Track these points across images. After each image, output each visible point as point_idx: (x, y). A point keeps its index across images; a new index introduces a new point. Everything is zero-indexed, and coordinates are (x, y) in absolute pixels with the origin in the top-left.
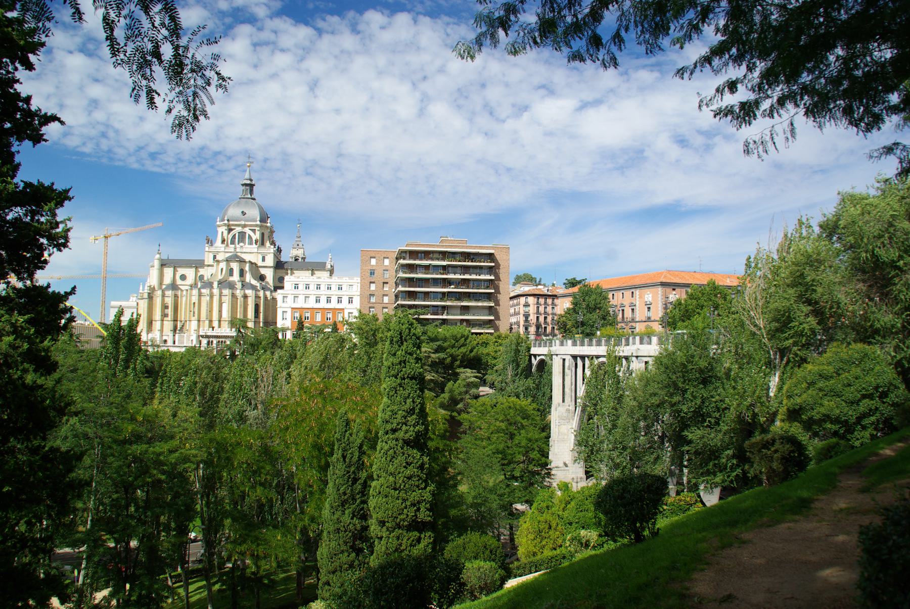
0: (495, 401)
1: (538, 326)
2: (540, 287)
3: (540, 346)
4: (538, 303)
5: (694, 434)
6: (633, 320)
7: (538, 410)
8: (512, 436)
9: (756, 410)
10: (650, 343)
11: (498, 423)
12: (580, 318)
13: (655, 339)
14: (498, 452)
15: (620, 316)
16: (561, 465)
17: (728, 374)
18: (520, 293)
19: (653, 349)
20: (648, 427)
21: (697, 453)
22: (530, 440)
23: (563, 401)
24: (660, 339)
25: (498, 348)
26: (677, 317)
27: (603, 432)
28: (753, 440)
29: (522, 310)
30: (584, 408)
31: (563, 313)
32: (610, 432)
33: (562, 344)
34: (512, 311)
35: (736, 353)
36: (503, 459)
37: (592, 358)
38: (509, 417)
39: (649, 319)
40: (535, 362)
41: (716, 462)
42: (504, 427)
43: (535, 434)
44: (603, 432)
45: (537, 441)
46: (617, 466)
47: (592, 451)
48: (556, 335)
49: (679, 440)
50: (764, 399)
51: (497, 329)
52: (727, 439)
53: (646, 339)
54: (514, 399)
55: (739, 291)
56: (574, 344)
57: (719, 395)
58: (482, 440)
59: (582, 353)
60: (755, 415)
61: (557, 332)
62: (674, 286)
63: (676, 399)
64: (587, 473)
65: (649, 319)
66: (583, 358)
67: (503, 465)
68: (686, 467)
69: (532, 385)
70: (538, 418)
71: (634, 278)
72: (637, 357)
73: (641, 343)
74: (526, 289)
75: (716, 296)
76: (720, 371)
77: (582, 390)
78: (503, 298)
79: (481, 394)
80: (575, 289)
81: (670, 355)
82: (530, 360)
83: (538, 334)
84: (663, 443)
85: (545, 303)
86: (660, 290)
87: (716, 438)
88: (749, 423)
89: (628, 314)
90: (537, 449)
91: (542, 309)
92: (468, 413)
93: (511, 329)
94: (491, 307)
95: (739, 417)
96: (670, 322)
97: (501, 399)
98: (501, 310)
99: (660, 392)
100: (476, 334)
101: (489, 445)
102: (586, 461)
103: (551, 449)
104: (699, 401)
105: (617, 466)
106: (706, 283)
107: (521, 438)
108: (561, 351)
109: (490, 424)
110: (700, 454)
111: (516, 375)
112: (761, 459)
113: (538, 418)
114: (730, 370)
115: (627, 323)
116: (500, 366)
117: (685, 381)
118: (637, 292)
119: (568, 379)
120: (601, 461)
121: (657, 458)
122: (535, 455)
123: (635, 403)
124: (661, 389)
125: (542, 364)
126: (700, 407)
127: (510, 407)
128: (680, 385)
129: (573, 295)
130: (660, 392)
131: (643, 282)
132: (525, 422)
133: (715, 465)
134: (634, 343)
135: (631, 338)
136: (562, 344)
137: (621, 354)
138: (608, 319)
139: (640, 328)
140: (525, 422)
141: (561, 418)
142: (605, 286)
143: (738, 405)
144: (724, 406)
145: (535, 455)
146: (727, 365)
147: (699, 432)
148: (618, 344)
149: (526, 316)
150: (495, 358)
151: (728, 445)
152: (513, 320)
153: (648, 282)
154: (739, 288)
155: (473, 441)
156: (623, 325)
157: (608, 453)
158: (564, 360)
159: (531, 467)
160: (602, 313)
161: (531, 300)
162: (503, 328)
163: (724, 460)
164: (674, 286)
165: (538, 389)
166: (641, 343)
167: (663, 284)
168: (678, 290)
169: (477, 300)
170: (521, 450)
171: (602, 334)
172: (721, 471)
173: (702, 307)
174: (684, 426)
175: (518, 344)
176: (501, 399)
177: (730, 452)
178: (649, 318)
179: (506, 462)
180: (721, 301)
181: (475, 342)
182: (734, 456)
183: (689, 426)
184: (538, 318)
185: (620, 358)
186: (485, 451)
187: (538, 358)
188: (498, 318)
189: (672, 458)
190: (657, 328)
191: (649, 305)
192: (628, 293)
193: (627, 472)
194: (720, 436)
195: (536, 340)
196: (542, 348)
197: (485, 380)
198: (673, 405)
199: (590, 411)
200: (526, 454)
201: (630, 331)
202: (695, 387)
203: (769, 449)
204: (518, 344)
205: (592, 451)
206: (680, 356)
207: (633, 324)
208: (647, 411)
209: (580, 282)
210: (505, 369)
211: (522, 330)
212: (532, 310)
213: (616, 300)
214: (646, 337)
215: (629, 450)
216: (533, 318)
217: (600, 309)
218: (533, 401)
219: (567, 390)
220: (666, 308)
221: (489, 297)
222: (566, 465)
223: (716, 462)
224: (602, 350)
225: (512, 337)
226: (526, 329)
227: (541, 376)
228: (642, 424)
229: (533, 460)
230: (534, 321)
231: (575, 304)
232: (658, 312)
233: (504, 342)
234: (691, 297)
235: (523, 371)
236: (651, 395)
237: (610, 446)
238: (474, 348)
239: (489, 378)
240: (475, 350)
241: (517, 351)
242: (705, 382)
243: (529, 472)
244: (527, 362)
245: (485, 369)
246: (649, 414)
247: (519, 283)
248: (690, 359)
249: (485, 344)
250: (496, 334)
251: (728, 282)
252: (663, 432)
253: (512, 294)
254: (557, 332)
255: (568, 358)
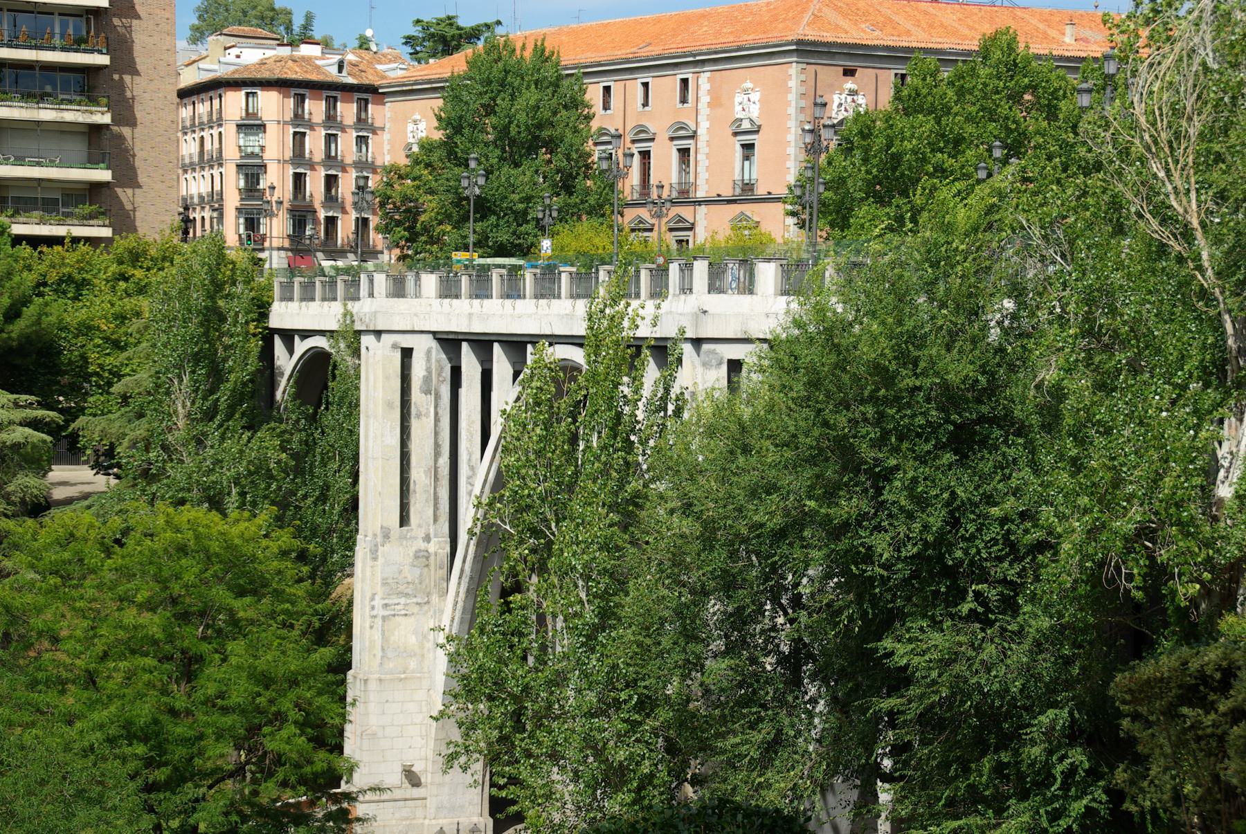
0: (116, 522)
1: (301, 215)
2: (306, 50)
3: (308, 296)
4: (298, 118)
5: (917, 646)
6: (685, 197)
7: (302, 557)
8: (190, 667)
9: (1163, 555)
10: (748, 288)
11: (130, 616)
12: (474, 185)
13: (767, 273)
14: (131, 733)
15: (635, 177)
16: (393, 777)
17: (1051, 418)
18: (222, 72)
19: (763, 309)
20: (738, 620)
21: (927, 720)
22: (266, 680)
23: (404, 520)
24: (786, 271)
25: (129, 304)
26: (855, 186)
27: (563, 644)
28: (1146, 670)
29: (233, 144)
30: (489, 539)
31: (403, 161)
32: (590, 640)
33: (398, 290)
34: (189, 148)
35: (1089, 330)
36: (149, 763)
37: (516, 345)
38: (176, 588)
39: (747, 193)
40: (286, 362)
41: (1005, 757)
42: (156, 631)
43: (287, 654)
44: (563, 644)
45: (294, 683)
46: (614, 777)
47: (517, 716)
48: (374, 253)
49: (860, 672)
50: (1193, 509)
51: (124, 222)
52: (1045, 665)
53: (733, 270)
54: (196, 513)
55: (1107, 79)
56: (449, 291)
57: (1016, 492)
58: (61, 685)
59: (478, 327)
60: (1158, 574)
61: (376, 239)
62: (852, 58)
63: (848, 507)
64: (496, 806)
65: (747, 193)
66: (483, 344)
67: (150, 788)
68: (887, 778)
69: (276, 457)
70: (300, 591)
71: (690, 20)
72: (697, 342)
73: (715, 286)
74: (251, 57)
75: (1015, 98)
76: (1023, 397)
77: (477, 473)
78: (150, 92)
79: (59, 494)
80: (455, 64)
81: (831, 334)
82: (267, 354)
83: (298, 246)
84: (795, 682)
85: (330, 118)
86: (793, 74)
87: (1004, 663)
88: (1137, 606)
89: (666, 169)
90: (294, 715)
91: (315, 144)
92: (425, 211)
93: (187, 222)
94: (95, 130)
95: (1094, 578)
96: (824, 208)
97: (141, 515)
98: (143, 142)
99: (787, 480)
100: (34, 241)
101: (91, 705)
102: (493, 759)
103: (354, 714)
104: (936, 518)
105: (614, 777)
106: (974, 46)
107: (228, 674)
108: (399, 315)
109: (98, 618)
110: (940, 725)
111: (209, 415)
112: (1179, 744)
113: (300, 591)
114: (1058, 393)
115: (659, 206)
116: (139, 379)
117: (885, 435)
118: (703, 82)
119: (422, 430)
120: (554, 756)
121: (773, 746)
122: (284, 740)
123: (687, 526)
124: (793, 467)
125: (318, 369)
126: (941, 540)
127: (182, 550)
128: (867, 453)
129: (450, 90)
130: (787, 480)
131: (727, 38)
132: (244, 608)
133: (999, 768)
134: (686, 289)
135: (674, 269)
136: (398, 290)
137: (644, 331)
138: (583, 189)
139: (710, 226)
140: (244, 608)
141: (392, 586)
142: (571, 56)
143: (1092, 533)
144: (1037, 535)
145: (284, 740)
146: (1049, 375)
147: (936, 638)
148: (625, 290)
149: (252, 171)
150: (118, 346)
151: (1052, 689)
152: (196, 186)
153: (749, 38)
154: (1111, 68)
155: (22, 693)
156: (644, 213)
157: (579, 725)
158: (407, 353)
159: (269, 791)
160: (559, 161)
161: (270, 104)
162: (154, 221)
163: (1036, 751)
164: (852, 58)
165: (299, 471)
166: (715, 286)
167: (808, 51)
168: (865, 75)
169: (38, 97)
170: (228, 720)
171: (559, 248)
172: (1024, 796)
173: (957, 144)
174: (885, 622)
175: (218, 286)
176: (141, 515)
177: (1055, 717)
178: (748, 187)
179: (161, 774)
180: (1034, 123)
181: (30, 278)
182: (1073, 735)
183: (902, 616)
184: (299, 179)
185: (637, 346)
186: (72, 732)
187: (301, 347)
188: (127, 175)
189: (835, 740)
190: (779, 225)
191: (746, 136)
192: (665, 86)
193: (655, 797)
194: (1019, 654)
195: (292, 270)
196: (315, 306)
197: (74, 437)
198: (838, 531)
199: (507, 568)
200: (249, 738)
201: (671, 239)
202: (922, 460)
203: (1210, 707)
204: (216, 287)
205: (517, 716)
206: (871, 342)
207: (686, 212)
208: (733, 555)
209: (472, 35)
210: (160, 389)
211: (232, 230)
212: (274, 145)
213: (615, 112)
214: (733, 265)
215: (664, 714)
216: (277, 180)
217: (551, 145)
218: (280, 521)
219: (419, 475)
220: (813, 149)
221: (85, 83)
222: (412, 778)
223: (1005, 757)
224: (563, 314)
225: (193, 255)
226: (252, 224)
227: (313, 419)
228: (714, 607)
229: (279, 760)
230: (285, 191)
231: (453, 125)
232: (781, 164)
233: (155, 277)
234: (909, 103)
235: (238, 398)
236: (753, 494)
237: (591, 697)
238: (26, 302)
239: (91, 427)
240: (29, 312)
241: (213, 318)
242: (964, 442)
243: (262, 812)
244: (253, 364)
245: (74, 390)
246: (744, 563)
247: (217, 30)
248: (908, 347)
249: (75, 286)
250: (122, 245)
251: (1068, 43)
252: (797, 642)
253: (189, 78)
254: (376, 239)
255: (424, 347)
